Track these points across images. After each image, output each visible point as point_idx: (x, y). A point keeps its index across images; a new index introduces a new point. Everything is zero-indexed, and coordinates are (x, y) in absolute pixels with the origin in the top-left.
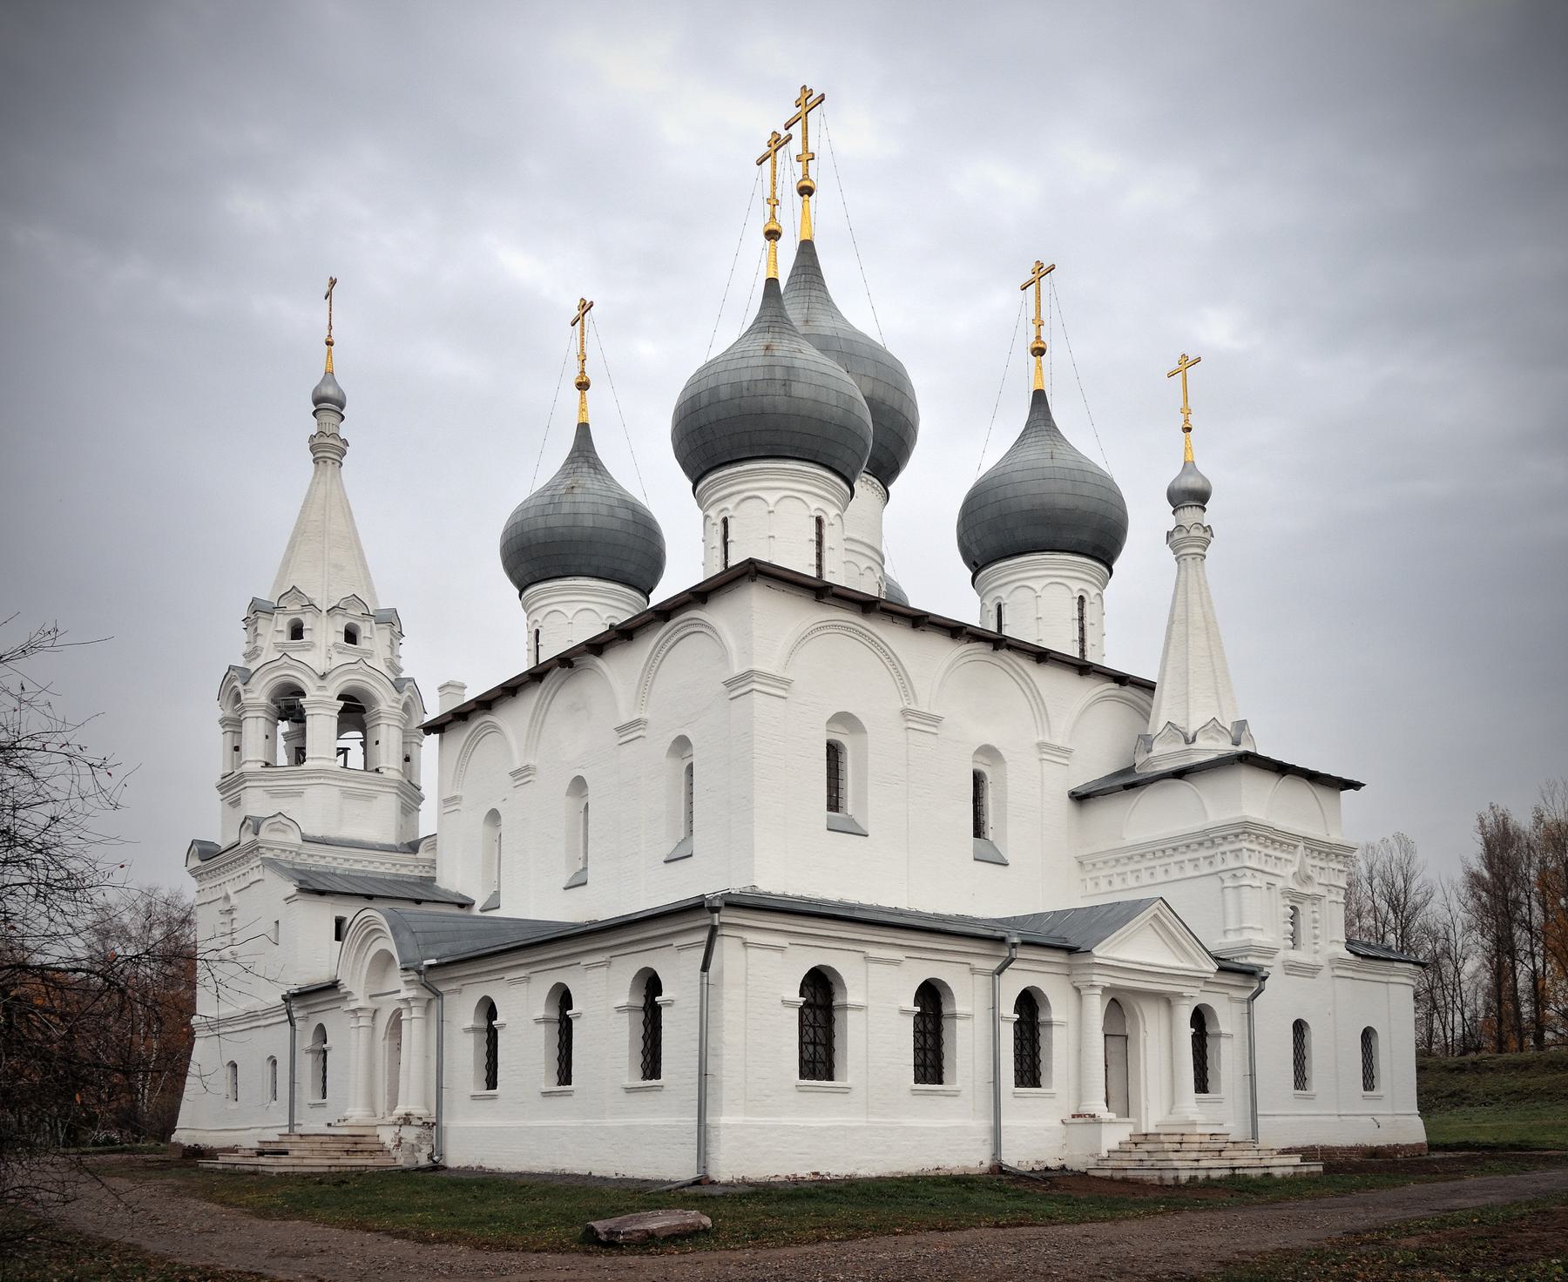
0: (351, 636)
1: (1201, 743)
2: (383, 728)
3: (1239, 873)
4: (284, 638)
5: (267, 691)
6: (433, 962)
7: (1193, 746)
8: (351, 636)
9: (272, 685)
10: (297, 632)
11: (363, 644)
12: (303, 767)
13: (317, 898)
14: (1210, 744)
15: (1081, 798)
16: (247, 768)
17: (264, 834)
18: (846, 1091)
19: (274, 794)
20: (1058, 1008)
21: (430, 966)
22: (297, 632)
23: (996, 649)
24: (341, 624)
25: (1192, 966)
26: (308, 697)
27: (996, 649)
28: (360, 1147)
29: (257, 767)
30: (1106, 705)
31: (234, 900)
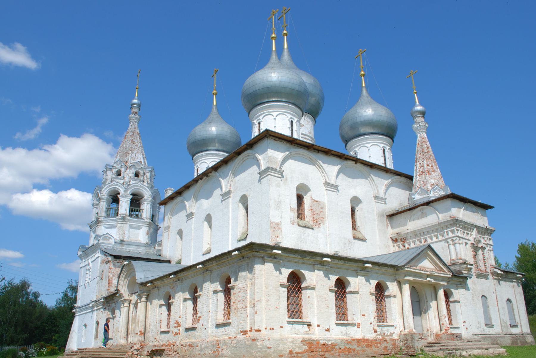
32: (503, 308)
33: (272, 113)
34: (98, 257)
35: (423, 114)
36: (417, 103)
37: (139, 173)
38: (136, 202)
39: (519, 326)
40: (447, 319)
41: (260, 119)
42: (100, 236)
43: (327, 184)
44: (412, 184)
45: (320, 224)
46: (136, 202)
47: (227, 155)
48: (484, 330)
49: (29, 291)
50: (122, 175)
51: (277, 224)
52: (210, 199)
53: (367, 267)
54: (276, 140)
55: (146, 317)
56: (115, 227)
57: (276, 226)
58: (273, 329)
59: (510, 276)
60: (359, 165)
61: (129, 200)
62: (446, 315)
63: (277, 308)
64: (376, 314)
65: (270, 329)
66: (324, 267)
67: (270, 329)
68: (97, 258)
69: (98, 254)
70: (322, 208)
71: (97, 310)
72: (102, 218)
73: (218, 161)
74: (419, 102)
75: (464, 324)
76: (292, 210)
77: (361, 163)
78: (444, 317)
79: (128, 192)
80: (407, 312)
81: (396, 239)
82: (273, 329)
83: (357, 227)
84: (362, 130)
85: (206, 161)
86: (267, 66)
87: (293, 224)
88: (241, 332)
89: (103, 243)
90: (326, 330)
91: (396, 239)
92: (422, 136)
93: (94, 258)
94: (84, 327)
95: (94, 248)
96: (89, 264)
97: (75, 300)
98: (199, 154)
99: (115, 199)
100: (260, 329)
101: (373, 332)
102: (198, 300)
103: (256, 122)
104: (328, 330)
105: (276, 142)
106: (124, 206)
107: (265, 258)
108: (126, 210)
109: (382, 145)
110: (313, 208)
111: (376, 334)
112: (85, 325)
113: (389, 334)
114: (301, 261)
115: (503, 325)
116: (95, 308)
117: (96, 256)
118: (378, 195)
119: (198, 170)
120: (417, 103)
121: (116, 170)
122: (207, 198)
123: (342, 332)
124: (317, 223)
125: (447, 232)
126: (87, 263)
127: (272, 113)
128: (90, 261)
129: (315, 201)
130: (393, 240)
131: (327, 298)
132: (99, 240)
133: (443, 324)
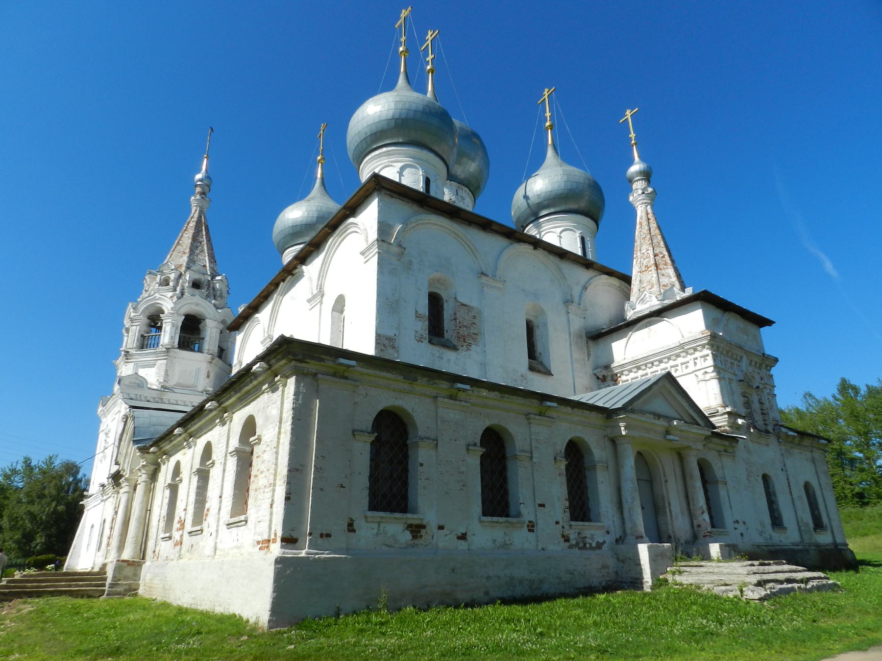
32: (800, 498)
36: (637, 159)
39: (829, 529)
40: (706, 516)
44: (630, 290)
45: (470, 345)
48: (771, 538)
49: (79, 476)
50: (171, 284)
51: (390, 339)
53: (549, 407)
54: (392, 197)
55: (687, 497)
56: (154, 366)
57: (387, 342)
58: (328, 535)
59: (807, 442)
60: (540, 253)
62: (705, 507)
63: (342, 486)
64: (567, 504)
65: (322, 536)
66: (458, 403)
67: (322, 536)
70: (474, 317)
72: (132, 351)
74: (639, 157)
75: (736, 525)
76: (418, 316)
77: (544, 249)
78: (700, 512)
80: (629, 501)
81: (604, 376)
82: (328, 535)
83: (537, 354)
87: (420, 340)
88: (258, 543)
90: (459, 538)
91: (604, 376)
92: (642, 210)
99: (154, 321)
100: (295, 536)
101: (562, 540)
104: (463, 537)
105: (393, 200)
106: (168, 334)
107: (319, 376)
108: (172, 338)
110: (458, 316)
111: (568, 544)
113: (594, 545)
114: (406, 386)
115: (803, 528)
120: (637, 159)
123: (495, 541)
124: (465, 341)
129: (463, 305)
130: (598, 378)
131: (463, 469)
133: (699, 526)
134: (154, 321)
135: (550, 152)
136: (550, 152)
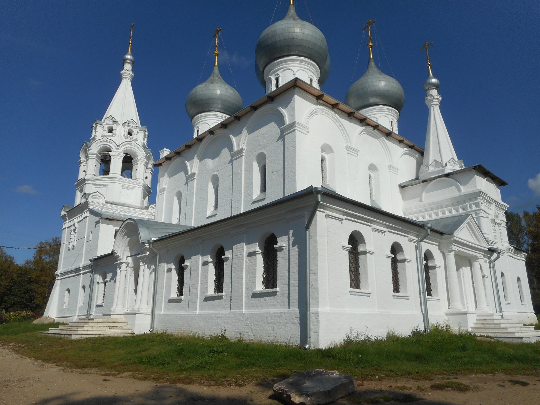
0: (130, 134)
1: (448, 166)
2: (139, 164)
3: (478, 212)
4: (106, 132)
5: (97, 149)
6: (156, 239)
7: (446, 168)
8: (130, 134)
9: (99, 148)
10: (111, 130)
11: (134, 136)
12: (108, 176)
13: (109, 221)
14: (451, 167)
15: (402, 187)
16: (88, 176)
17: (90, 199)
18: (368, 295)
19: (96, 186)
20: (438, 259)
21: (155, 241)
22: (111, 130)
23: (374, 129)
24: (127, 128)
25: (477, 243)
26: (112, 152)
27: (374, 129)
28: (116, 324)
29: (91, 176)
30: (407, 156)
31: (77, 225)
33: (206, 122)
34: (86, 217)
35: (437, 86)
37: (133, 131)
38: (128, 161)
41: (278, 74)
42: (89, 195)
43: (347, 147)
46: (128, 161)
47: (229, 117)
52: (217, 159)
61: (122, 158)
68: (84, 218)
69: (87, 214)
71: (83, 274)
73: (219, 122)
79: (121, 150)
84: (372, 100)
85: (208, 121)
86: (208, 80)
89: (92, 202)
93: (81, 218)
94: (67, 292)
95: (84, 207)
96: (74, 225)
97: (54, 265)
98: (278, 60)
99: (105, 162)
102: (225, 263)
103: (273, 78)
106: (116, 165)
109: (391, 117)
112: (68, 290)
116: (82, 272)
117: (84, 216)
118: (400, 162)
119: (198, 131)
121: (108, 126)
122: (213, 158)
125: (470, 205)
126: (72, 223)
127: (206, 122)
128: (76, 221)
132: (87, 199)
134: (105, 162)
135: (372, 64)
136: (372, 64)
